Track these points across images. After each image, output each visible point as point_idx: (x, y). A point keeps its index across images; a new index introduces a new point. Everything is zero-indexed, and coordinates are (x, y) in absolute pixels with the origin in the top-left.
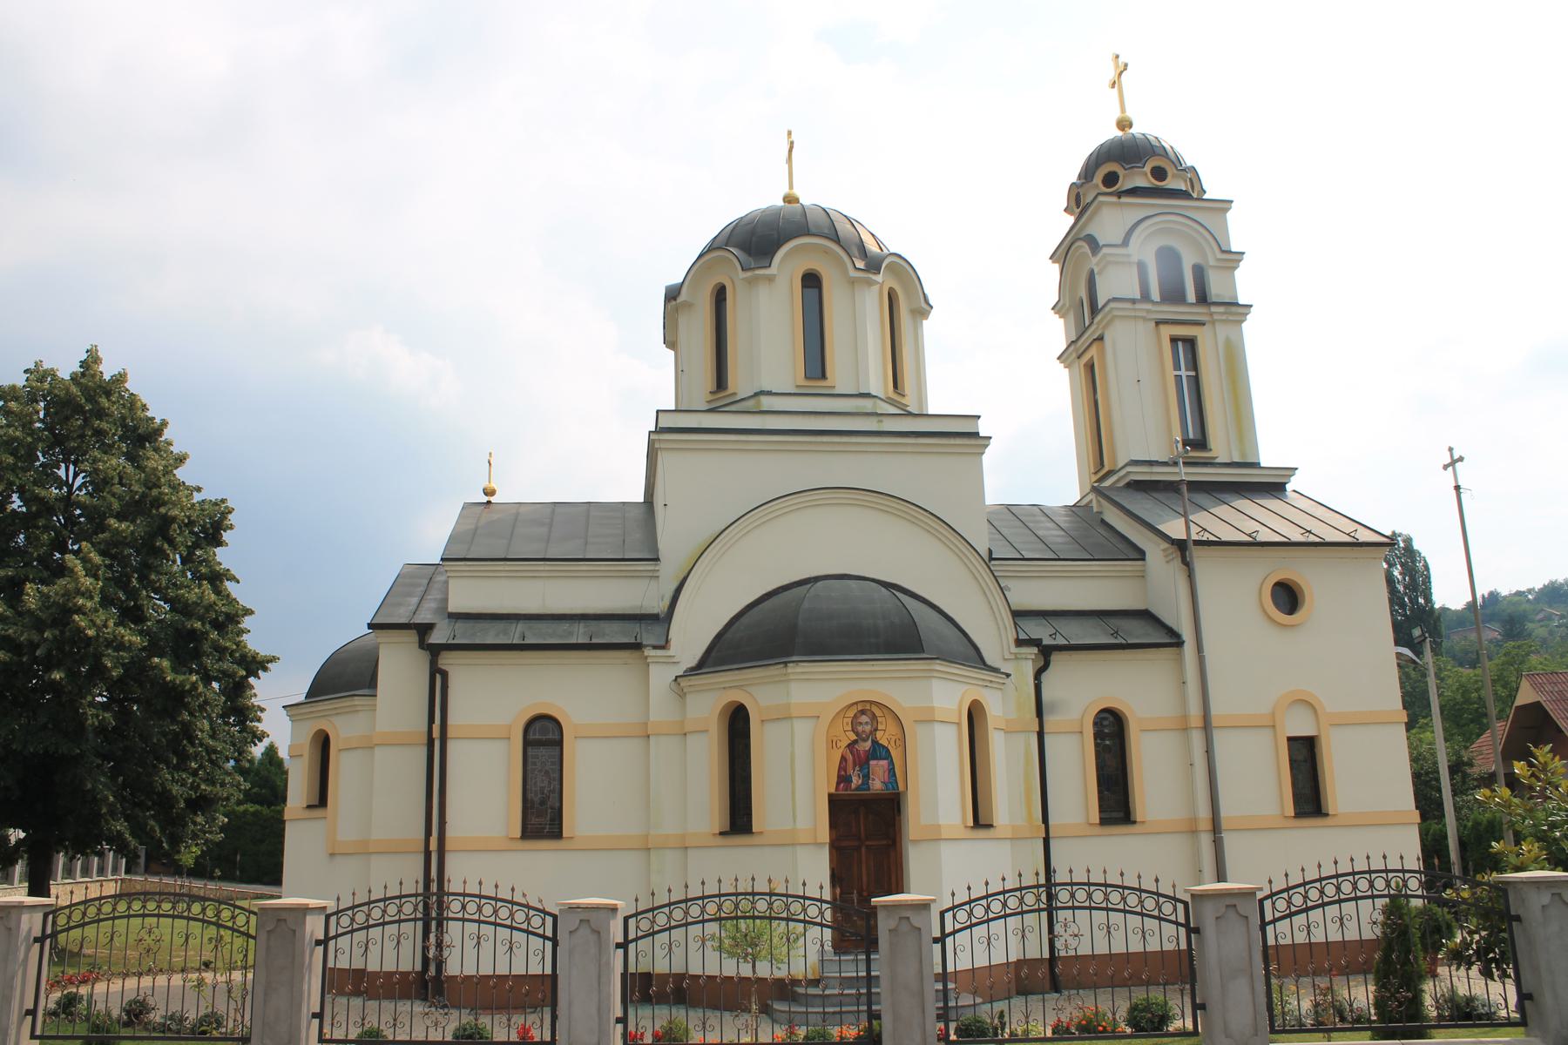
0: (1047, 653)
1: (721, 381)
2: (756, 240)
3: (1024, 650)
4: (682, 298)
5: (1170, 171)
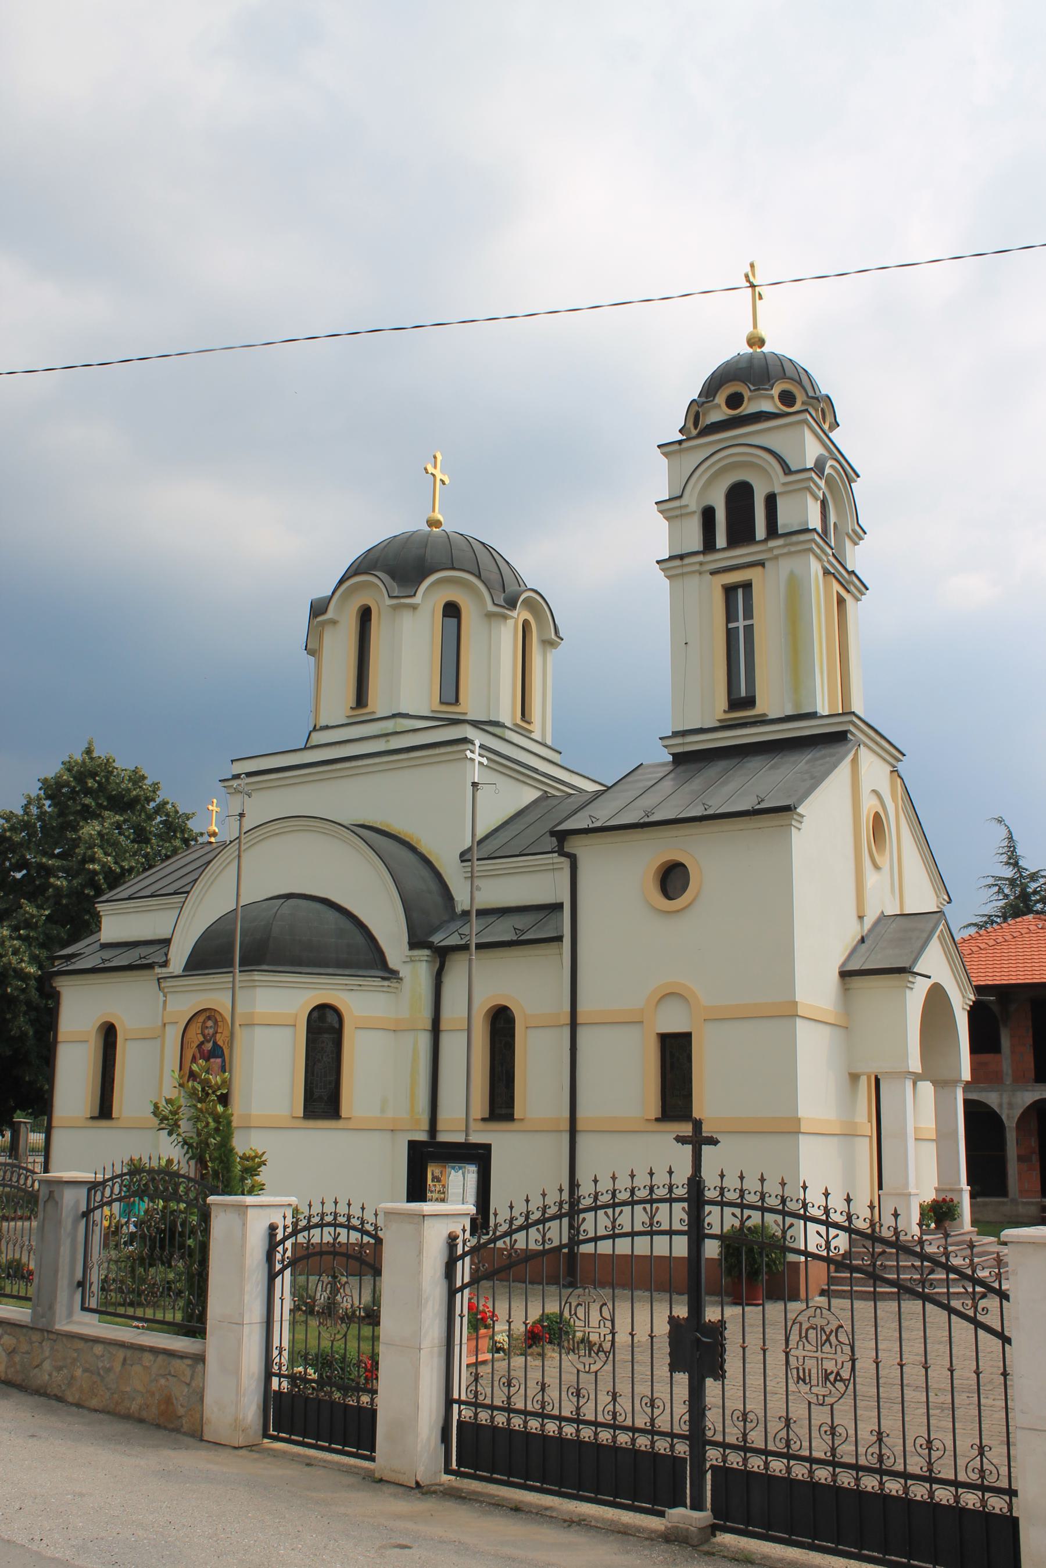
1: (361, 699)
2: (402, 565)
3: (416, 953)
4: (330, 614)
5: (800, 398)
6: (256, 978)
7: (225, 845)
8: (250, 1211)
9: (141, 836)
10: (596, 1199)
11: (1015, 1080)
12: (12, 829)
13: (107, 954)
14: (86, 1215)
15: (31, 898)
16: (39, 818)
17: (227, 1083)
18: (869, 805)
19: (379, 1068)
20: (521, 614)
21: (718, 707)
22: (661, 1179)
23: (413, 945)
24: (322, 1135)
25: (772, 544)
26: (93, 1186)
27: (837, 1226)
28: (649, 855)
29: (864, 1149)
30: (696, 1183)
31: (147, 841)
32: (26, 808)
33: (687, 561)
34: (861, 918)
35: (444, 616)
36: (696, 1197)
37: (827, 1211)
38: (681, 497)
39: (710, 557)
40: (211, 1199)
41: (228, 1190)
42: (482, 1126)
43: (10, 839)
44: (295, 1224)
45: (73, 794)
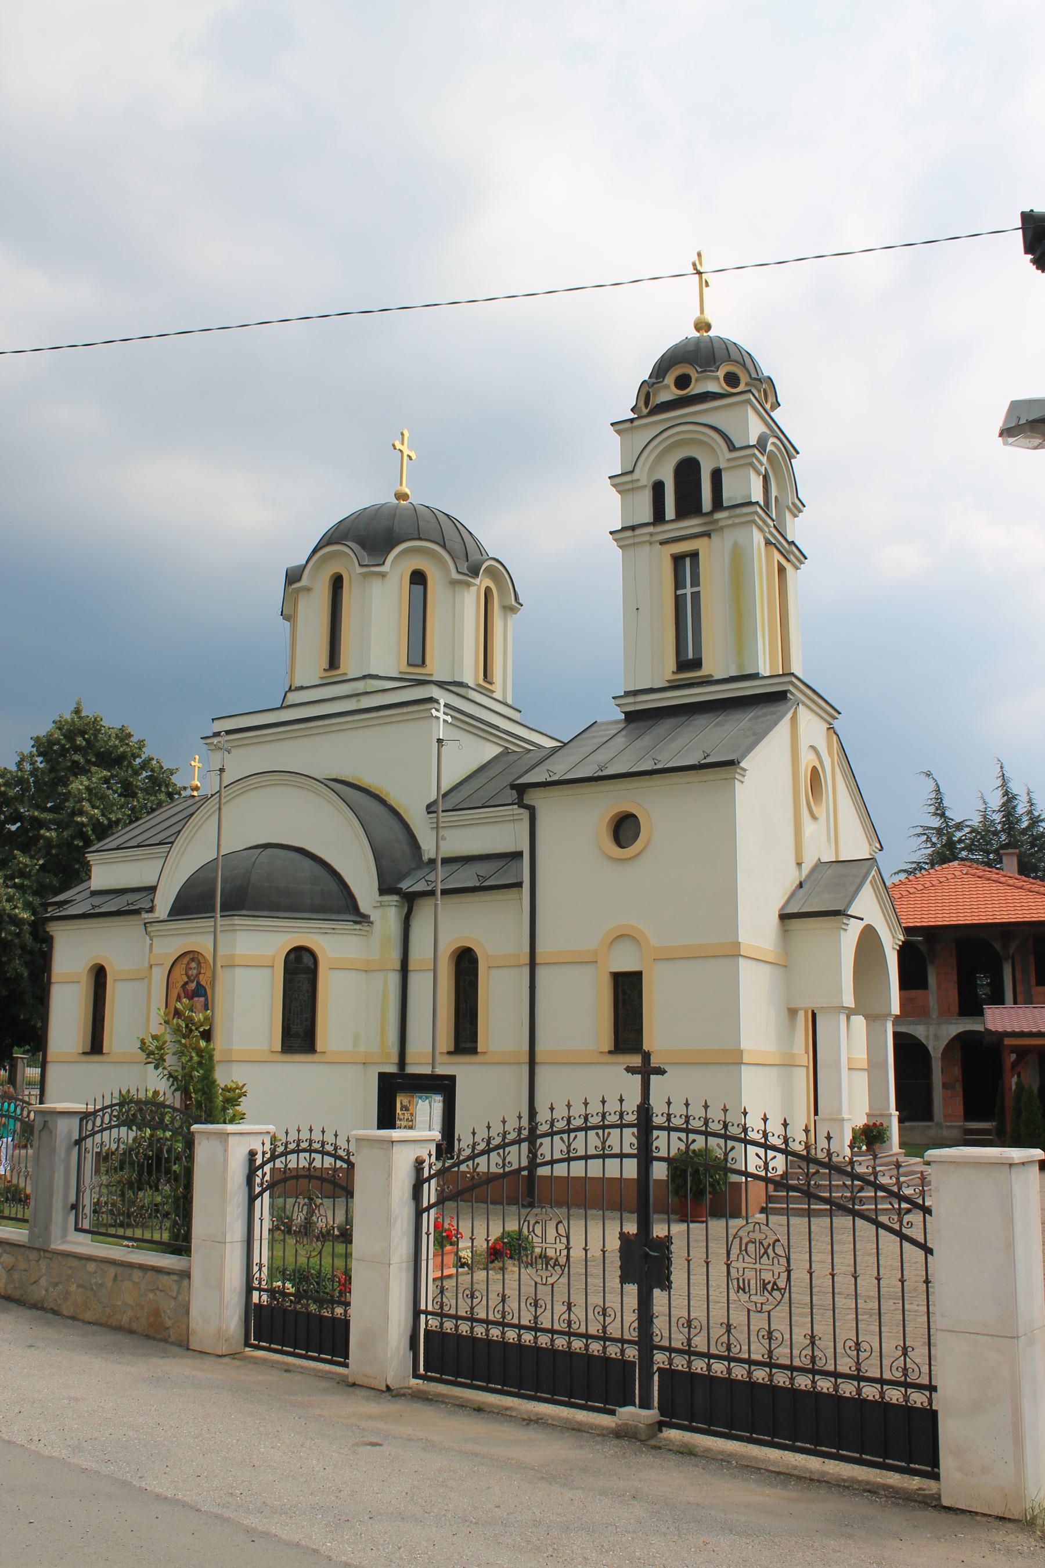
0: (410, 900)
1: (333, 662)
2: (371, 536)
3: (386, 898)
4: (304, 582)
5: (744, 379)
6: (237, 922)
7: (206, 799)
8: (232, 1140)
9: (128, 791)
10: (552, 1125)
11: (941, 1014)
13: (97, 900)
14: (78, 1142)
15: (25, 850)
17: (209, 1020)
18: (807, 759)
20: (483, 581)
21: (666, 669)
23: (383, 891)
24: (299, 1069)
25: (718, 515)
27: (774, 1148)
28: (599, 809)
29: (802, 1078)
30: (645, 1111)
31: (134, 795)
32: (19, 764)
33: (638, 532)
34: (799, 864)
35: (411, 583)
38: (632, 472)
40: (195, 1127)
41: (210, 1119)
44: (273, 1151)
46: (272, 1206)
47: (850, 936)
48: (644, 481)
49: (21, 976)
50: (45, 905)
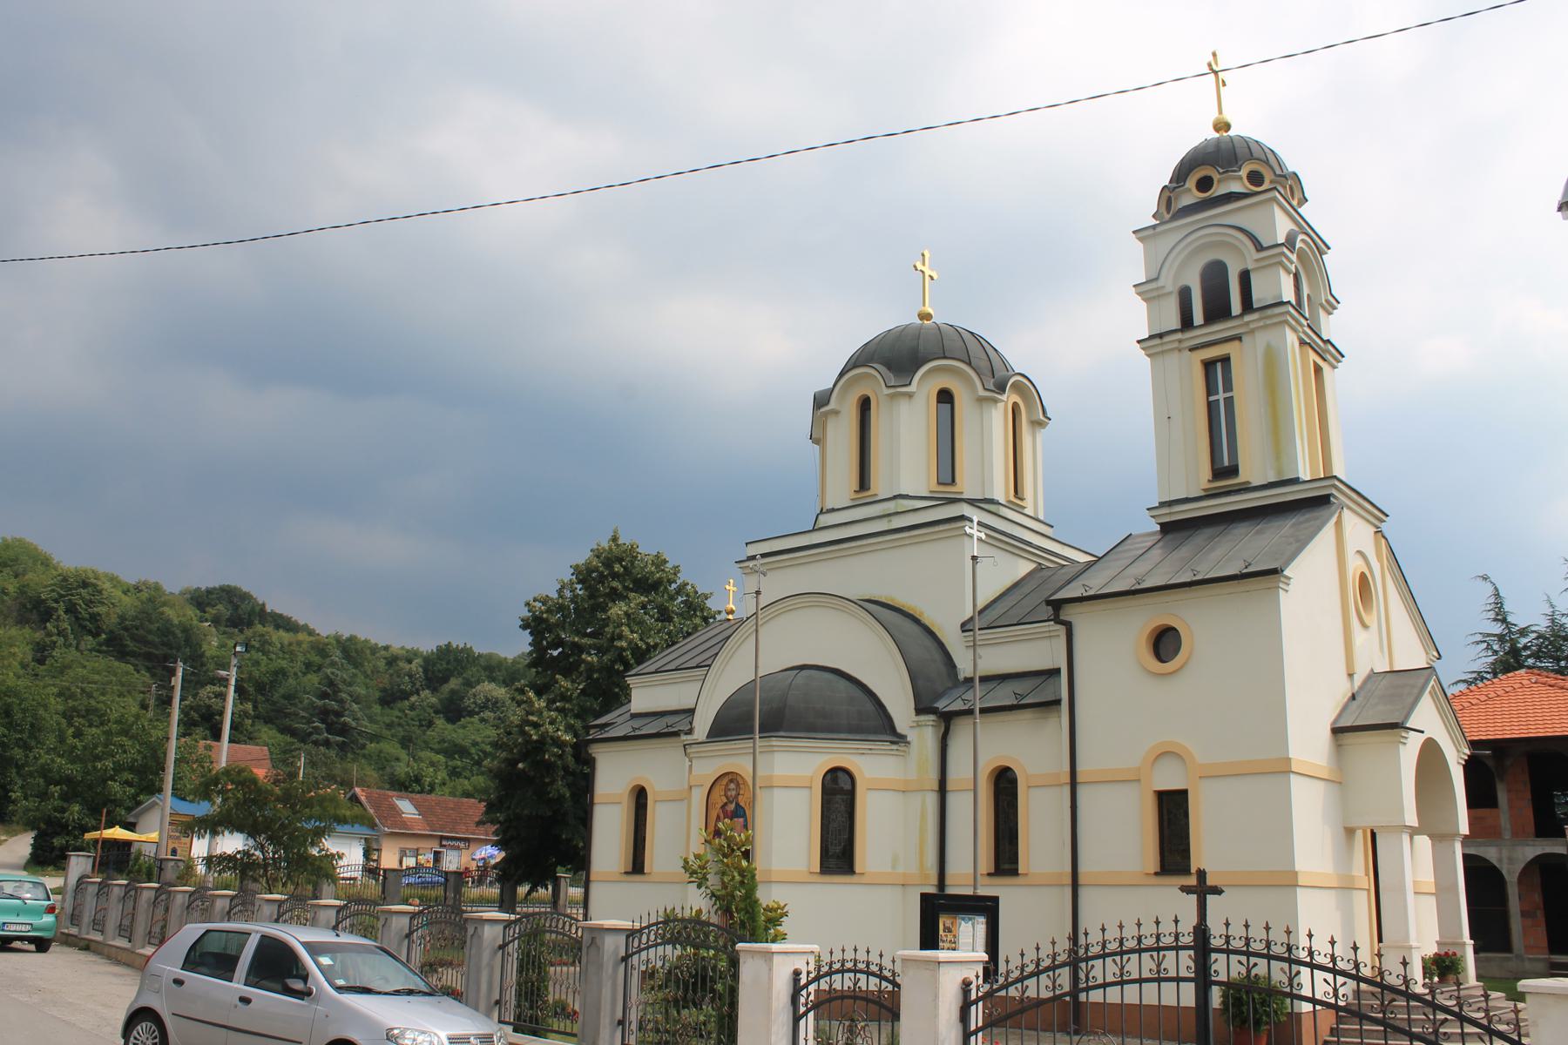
1: (864, 483)
2: (897, 357)
4: (832, 405)
5: (1268, 177)
7: (742, 622)
8: (776, 959)
9: (665, 615)
10: (1104, 947)
11: (1515, 834)
12: (549, 611)
13: (637, 723)
14: (625, 959)
15: (566, 673)
16: (572, 601)
17: (750, 840)
18: (1355, 566)
19: (889, 826)
20: (1010, 397)
21: (1202, 477)
22: (1167, 927)
23: (919, 711)
24: (837, 890)
25: (1247, 318)
26: (631, 934)
27: (1344, 973)
28: (1141, 620)
29: (1362, 903)
30: (1201, 932)
31: (670, 620)
32: (560, 591)
33: (1166, 339)
34: (1351, 675)
36: (1202, 944)
37: (1333, 959)
38: (1156, 279)
39: (1188, 335)
40: (740, 946)
41: (754, 938)
42: (988, 880)
43: (546, 620)
44: (819, 968)
45: (602, 579)
46: (817, 1030)
47: (1409, 752)
48: (1169, 288)
49: (563, 796)
50: (587, 728)
